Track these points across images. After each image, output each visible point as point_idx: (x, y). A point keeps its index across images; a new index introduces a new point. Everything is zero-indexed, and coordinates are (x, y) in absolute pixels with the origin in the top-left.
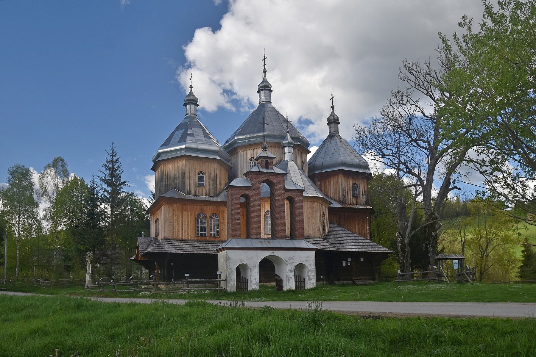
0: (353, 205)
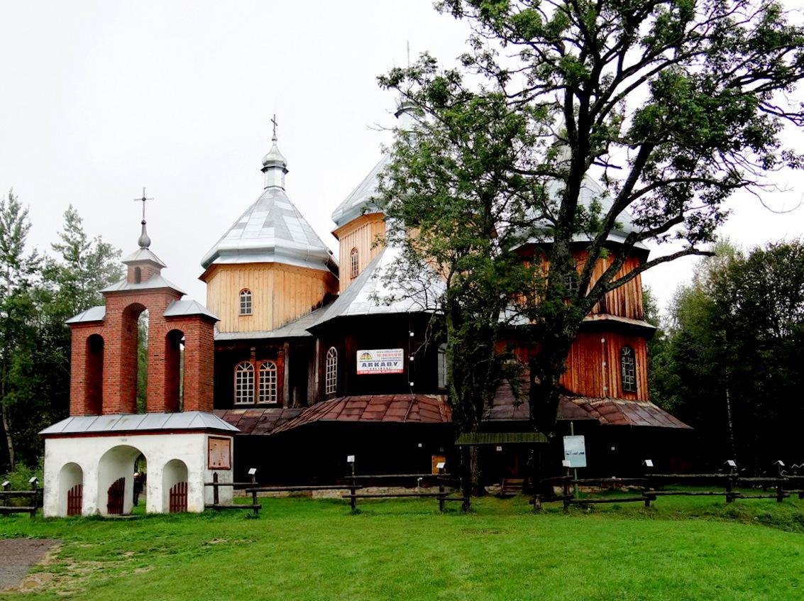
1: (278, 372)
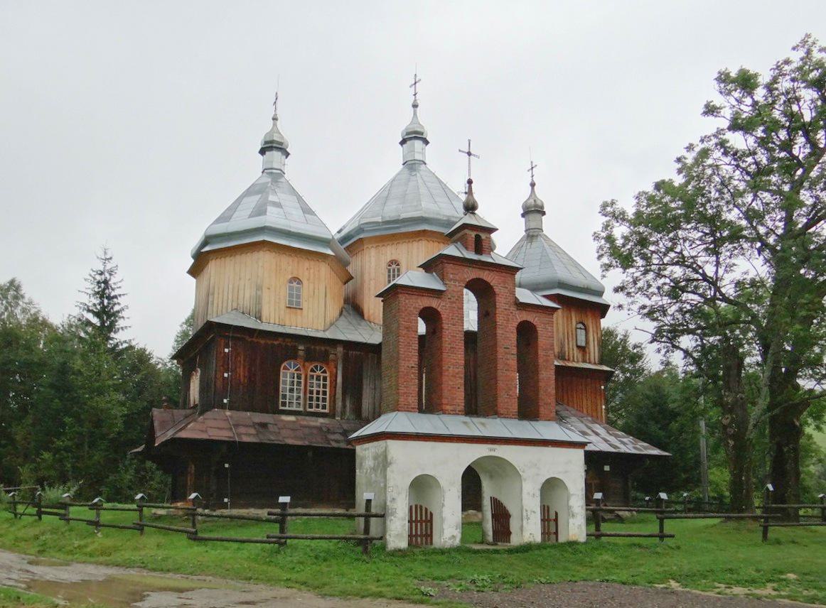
0: (578, 362)
1: (331, 377)
